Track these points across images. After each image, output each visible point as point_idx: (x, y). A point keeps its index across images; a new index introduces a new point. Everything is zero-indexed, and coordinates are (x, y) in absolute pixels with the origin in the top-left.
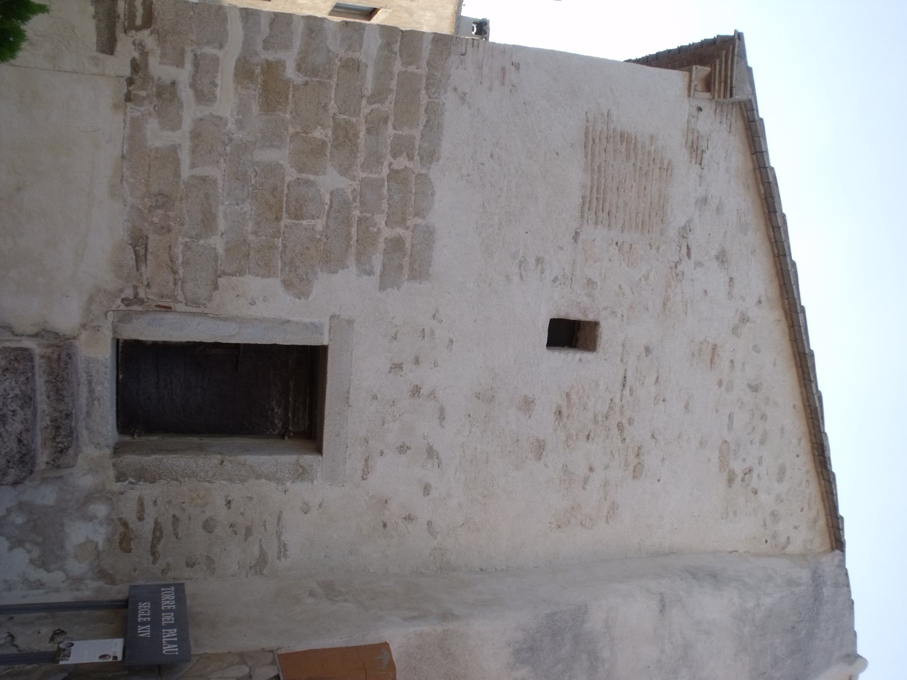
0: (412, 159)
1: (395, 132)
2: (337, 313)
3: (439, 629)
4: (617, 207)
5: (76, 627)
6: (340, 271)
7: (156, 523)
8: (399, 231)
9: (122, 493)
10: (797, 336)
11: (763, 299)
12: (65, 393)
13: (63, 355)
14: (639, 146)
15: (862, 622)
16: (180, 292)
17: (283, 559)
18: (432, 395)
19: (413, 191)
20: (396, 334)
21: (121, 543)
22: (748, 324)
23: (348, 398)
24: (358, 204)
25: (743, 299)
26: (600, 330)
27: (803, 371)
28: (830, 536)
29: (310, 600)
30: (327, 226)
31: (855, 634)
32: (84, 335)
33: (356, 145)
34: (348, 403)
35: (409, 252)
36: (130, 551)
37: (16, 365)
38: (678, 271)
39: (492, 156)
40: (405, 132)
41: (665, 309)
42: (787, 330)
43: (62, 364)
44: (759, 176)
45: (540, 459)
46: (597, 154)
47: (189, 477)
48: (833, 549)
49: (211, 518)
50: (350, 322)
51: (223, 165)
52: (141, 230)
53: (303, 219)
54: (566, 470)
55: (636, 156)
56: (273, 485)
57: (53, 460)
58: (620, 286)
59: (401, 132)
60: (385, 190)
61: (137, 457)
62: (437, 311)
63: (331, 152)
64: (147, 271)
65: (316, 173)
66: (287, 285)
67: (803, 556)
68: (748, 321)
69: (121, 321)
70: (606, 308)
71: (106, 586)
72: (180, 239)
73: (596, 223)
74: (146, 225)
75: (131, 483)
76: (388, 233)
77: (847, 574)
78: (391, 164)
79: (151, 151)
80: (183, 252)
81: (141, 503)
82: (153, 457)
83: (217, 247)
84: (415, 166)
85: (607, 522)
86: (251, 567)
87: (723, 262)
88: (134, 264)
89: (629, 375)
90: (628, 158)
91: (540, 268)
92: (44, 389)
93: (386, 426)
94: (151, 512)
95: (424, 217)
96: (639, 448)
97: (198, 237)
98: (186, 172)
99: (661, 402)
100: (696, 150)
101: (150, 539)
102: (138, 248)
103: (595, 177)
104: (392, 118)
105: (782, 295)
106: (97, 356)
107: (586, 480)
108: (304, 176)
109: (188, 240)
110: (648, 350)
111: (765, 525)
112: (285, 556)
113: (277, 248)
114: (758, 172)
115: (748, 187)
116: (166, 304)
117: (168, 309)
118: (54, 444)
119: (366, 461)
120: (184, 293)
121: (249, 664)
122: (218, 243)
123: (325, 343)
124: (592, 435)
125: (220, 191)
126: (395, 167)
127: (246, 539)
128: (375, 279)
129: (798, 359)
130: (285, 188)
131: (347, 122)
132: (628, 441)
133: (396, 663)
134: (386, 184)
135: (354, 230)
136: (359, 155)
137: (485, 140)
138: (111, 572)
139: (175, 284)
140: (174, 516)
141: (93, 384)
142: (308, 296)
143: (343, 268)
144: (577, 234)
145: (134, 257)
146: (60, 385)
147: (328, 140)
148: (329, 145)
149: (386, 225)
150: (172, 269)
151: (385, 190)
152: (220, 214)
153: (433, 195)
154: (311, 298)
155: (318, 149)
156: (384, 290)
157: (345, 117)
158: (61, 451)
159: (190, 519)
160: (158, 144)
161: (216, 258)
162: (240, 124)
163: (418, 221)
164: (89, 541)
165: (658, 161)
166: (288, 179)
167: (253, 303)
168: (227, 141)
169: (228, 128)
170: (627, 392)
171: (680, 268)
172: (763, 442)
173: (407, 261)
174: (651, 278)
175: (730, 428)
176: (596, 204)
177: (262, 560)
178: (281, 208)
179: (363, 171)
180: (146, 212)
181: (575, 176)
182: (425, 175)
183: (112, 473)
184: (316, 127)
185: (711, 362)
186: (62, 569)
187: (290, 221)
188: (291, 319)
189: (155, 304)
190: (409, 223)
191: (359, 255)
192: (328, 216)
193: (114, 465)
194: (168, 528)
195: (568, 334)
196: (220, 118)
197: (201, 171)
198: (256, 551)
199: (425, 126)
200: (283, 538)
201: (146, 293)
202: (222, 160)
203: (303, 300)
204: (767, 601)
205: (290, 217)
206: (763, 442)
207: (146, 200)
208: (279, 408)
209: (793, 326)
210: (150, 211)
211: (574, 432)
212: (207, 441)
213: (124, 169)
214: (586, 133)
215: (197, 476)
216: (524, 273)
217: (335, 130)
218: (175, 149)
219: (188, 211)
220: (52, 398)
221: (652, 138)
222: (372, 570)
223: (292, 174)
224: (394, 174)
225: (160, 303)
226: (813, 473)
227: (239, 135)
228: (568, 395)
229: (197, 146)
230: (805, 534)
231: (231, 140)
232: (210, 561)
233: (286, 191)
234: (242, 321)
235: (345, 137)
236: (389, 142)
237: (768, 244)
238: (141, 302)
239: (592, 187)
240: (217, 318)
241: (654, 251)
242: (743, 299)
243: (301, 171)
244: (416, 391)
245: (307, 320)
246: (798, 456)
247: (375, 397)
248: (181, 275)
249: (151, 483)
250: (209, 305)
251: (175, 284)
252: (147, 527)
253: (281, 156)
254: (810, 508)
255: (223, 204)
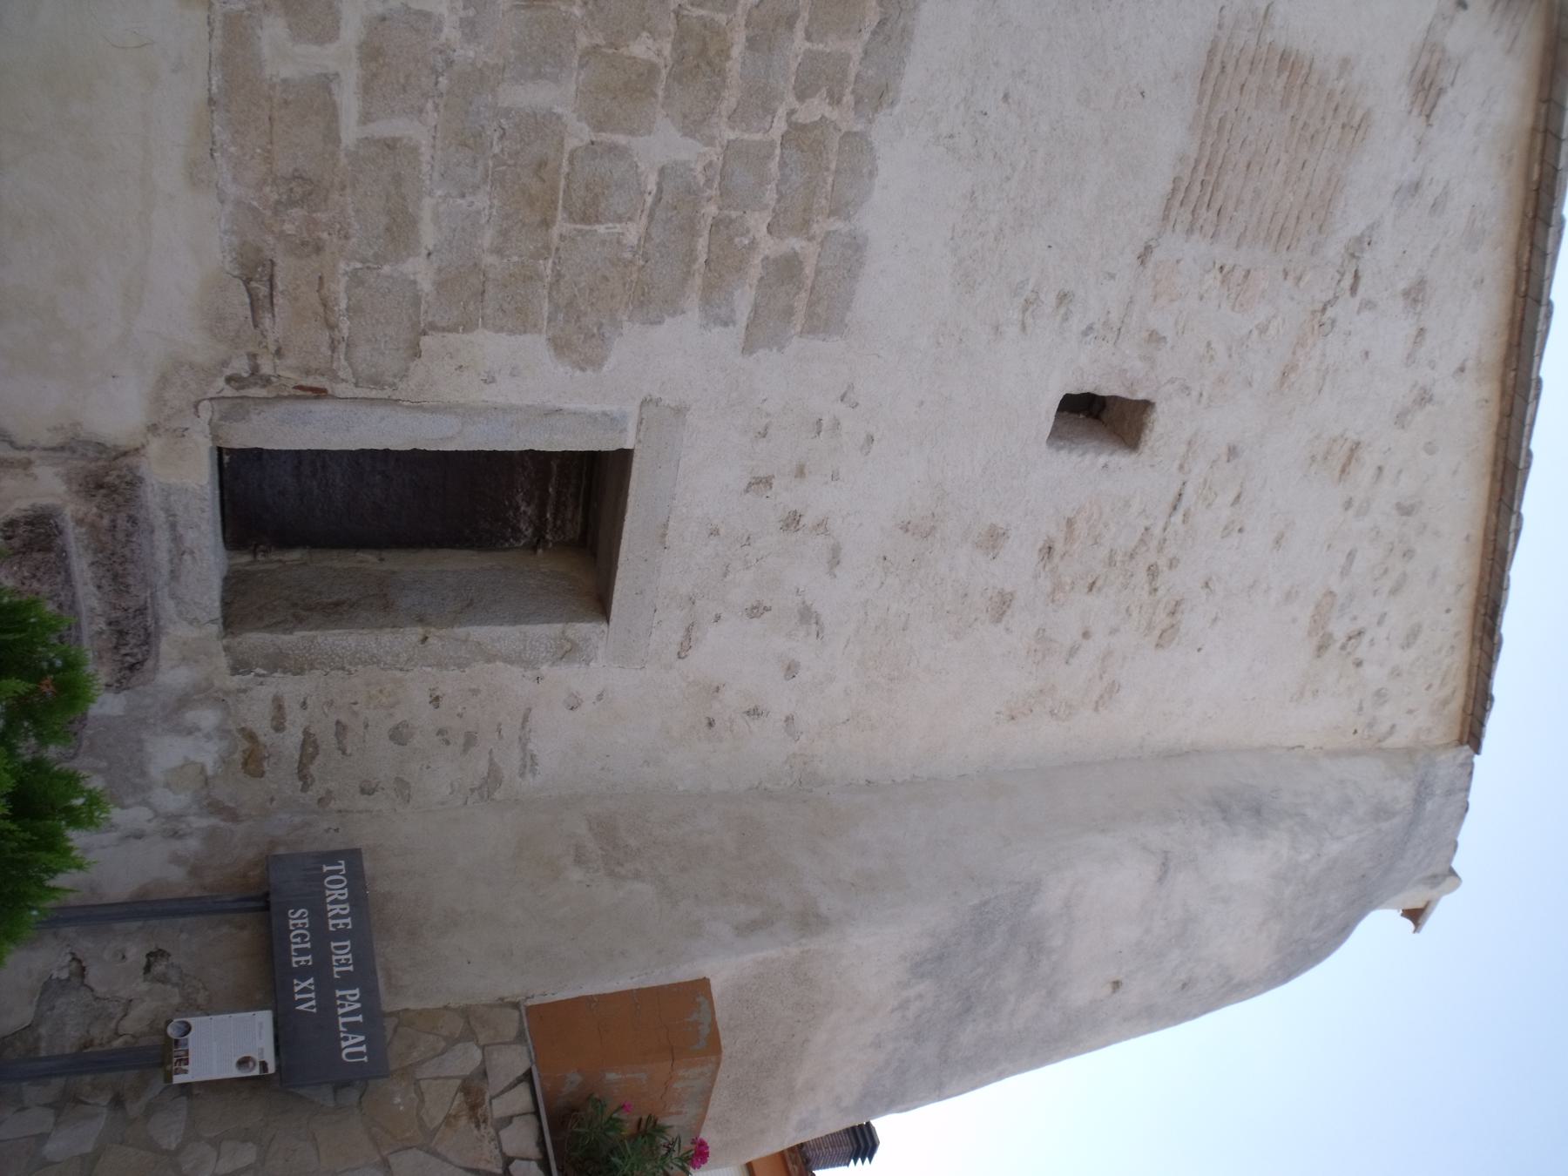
0: (839, 101)
1: (808, 45)
2: (656, 395)
3: (794, 951)
4: (1239, 201)
5: (184, 936)
6: (668, 320)
7: (306, 733)
8: (795, 243)
9: (245, 691)
10: (1513, 434)
11: (1470, 364)
12: (130, 580)
13: (122, 523)
14: (1313, 80)
15: (1468, 834)
16: (343, 362)
17: (529, 776)
18: (822, 526)
19: (833, 166)
20: (766, 428)
21: (245, 764)
22: (1429, 407)
23: (664, 535)
24: (714, 192)
25: (1432, 365)
26: (1154, 416)
27: (1502, 490)
28: (1463, 725)
29: (576, 874)
30: (648, 237)
31: (1456, 846)
32: (155, 447)
33: (721, 73)
34: (663, 543)
35: (809, 283)
36: (262, 774)
37: (36, 585)
38: (1325, 319)
39: (1006, 97)
40: (831, 45)
41: (1282, 384)
42: (1496, 418)
43: (121, 536)
44: (1538, 148)
45: (999, 620)
46: (1223, 95)
47: (365, 663)
48: (1461, 742)
49: (405, 724)
50: (680, 411)
51: (432, 117)
52: (259, 250)
53: (598, 222)
54: (1041, 635)
55: (1301, 103)
56: (516, 670)
57: (118, 681)
58: (1209, 344)
59: (821, 46)
60: (774, 166)
61: (267, 636)
62: (851, 387)
63: (667, 89)
64: (276, 327)
65: (632, 132)
66: (560, 346)
67: (1410, 752)
68: (1430, 400)
69: (225, 417)
70: (1172, 381)
71: (222, 824)
72: (342, 266)
73: (1190, 231)
74: (270, 239)
75: (258, 675)
76: (770, 247)
77: (1471, 773)
78: (792, 112)
79: (272, 87)
80: (348, 289)
81: (278, 705)
82: (298, 635)
83: (419, 278)
84: (844, 118)
85: (1096, 709)
86: (472, 790)
87: (1415, 301)
88: (249, 313)
89: (1189, 491)
90: (1285, 104)
91: (1062, 310)
92: (88, 575)
93: (729, 578)
94: (296, 722)
95: (848, 218)
96: (1178, 604)
97: (380, 259)
98: (350, 131)
99: (1235, 533)
100: (1427, 89)
101: (297, 757)
102: (253, 284)
103: (1210, 141)
104: (805, 15)
105: (1506, 362)
106: (184, 482)
107: (1073, 651)
108: (605, 137)
109: (359, 265)
110: (1233, 452)
111: (1361, 709)
112: (534, 772)
113: (541, 278)
114: (1539, 138)
115: (1510, 160)
116: (315, 385)
117: (319, 393)
118: (118, 657)
119: (688, 630)
120: (351, 365)
121: (483, 1040)
122: (421, 271)
123: (628, 446)
124: (1098, 584)
125: (425, 168)
126: (801, 118)
127: (465, 751)
128: (737, 333)
129: (1501, 467)
130: (565, 163)
131: (706, 24)
132: (1160, 593)
133: (722, 1034)
134: (778, 151)
135: (702, 243)
136: (726, 94)
137: (996, 64)
138: (232, 805)
139: (333, 348)
140: (338, 723)
141: (180, 530)
142: (601, 366)
143: (673, 315)
144: (1148, 249)
145: (247, 300)
146: (119, 569)
147: (661, 62)
148: (664, 73)
149: (769, 232)
150: (326, 320)
151: (774, 166)
152: (426, 215)
153: (872, 174)
154: (605, 369)
155: (639, 84)
156: (751, 353)
157: (702, 12)
158: (132, 667)
159: (366, 726)
160: (287, 71)
161: (416, 301)
162: (470, 29)
163: (837, 225)
164: (188, 762)
165: (1343, 112)
166: (571, 143)
167: (490, 380)
168: (440, 65)
169: (443, 39)
170: (1178, 518)
171: (1330, 312)
172: (1395, 591)
173: (806, 299)
174: (1272, 331)
175: (1345, 572)
176: (1198, 196)
177: (494, 777)
178: (554, 202)
179: (733, 129)
180: (268, 213)
181: (1168, 137)
182: (863, 136)
183: (223, 662)
184: (638, 35)
185: (1343, 471)
186: (145, 803)
187: (571, 226)
188: (566, 406)
189: (293, 384)
190: (815, 228)
191: (709, 288)
192: (651, 216)
193: (227, 649)
194: (327, 740)
195: (1097, 417)
196: (427, 16)
197: (384, 128)
198: (483, 766)
199: (874, 33)
200: (530, 746)
201: (275, 367)
202: (430, 105)
203: (589, 372)
204: (1334, 848)
205: (571, 218)
206: (1395, 591)
207: (267, 189)
208: (529, 504)
209: (1510, 416)
210: (276, 213)
211: (1068, 580)
212: (398, 563)
213: (217, 128)
214: (1211, 53)
215: (378, 662)
216: (1029, 321)
217: (679, 41)
218: (326, 82)
219: (357, 211)
220: (107, 588)
221: (1345, 64)
222: (681, 788)
223: (579, 134)
224: (797, 133)
225: (303, 383)
226: (1466, 636)
227: (467, 53)
228: (1070, 523)
229: (375, 76)
230: (1419, 714)
231: (450, 63)
232: (402, 785)
233: (565, 168)
234: (467, 412)
235: (699, 57)
236: (794, 66)
237: (1511, 269)
238: (267, 381)
239: (1197, 161)
240: (418, 407)
241: (1290, 282)
242: (1432, 365)
243: (599, 127)
244: (792, 521)
245: (596, 408)
246: (1448, 611)
247: (715, 532)
248: (346, 333)
249: (295, 674)
250: (401, 386)
251: (333, 348)
252: (292, 740)
253: (555, 96)
254: (1443, 684)
255: (430, 194)
